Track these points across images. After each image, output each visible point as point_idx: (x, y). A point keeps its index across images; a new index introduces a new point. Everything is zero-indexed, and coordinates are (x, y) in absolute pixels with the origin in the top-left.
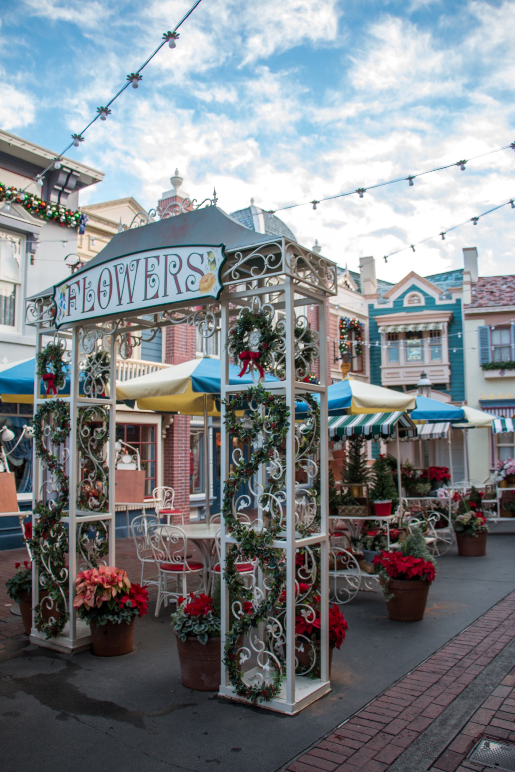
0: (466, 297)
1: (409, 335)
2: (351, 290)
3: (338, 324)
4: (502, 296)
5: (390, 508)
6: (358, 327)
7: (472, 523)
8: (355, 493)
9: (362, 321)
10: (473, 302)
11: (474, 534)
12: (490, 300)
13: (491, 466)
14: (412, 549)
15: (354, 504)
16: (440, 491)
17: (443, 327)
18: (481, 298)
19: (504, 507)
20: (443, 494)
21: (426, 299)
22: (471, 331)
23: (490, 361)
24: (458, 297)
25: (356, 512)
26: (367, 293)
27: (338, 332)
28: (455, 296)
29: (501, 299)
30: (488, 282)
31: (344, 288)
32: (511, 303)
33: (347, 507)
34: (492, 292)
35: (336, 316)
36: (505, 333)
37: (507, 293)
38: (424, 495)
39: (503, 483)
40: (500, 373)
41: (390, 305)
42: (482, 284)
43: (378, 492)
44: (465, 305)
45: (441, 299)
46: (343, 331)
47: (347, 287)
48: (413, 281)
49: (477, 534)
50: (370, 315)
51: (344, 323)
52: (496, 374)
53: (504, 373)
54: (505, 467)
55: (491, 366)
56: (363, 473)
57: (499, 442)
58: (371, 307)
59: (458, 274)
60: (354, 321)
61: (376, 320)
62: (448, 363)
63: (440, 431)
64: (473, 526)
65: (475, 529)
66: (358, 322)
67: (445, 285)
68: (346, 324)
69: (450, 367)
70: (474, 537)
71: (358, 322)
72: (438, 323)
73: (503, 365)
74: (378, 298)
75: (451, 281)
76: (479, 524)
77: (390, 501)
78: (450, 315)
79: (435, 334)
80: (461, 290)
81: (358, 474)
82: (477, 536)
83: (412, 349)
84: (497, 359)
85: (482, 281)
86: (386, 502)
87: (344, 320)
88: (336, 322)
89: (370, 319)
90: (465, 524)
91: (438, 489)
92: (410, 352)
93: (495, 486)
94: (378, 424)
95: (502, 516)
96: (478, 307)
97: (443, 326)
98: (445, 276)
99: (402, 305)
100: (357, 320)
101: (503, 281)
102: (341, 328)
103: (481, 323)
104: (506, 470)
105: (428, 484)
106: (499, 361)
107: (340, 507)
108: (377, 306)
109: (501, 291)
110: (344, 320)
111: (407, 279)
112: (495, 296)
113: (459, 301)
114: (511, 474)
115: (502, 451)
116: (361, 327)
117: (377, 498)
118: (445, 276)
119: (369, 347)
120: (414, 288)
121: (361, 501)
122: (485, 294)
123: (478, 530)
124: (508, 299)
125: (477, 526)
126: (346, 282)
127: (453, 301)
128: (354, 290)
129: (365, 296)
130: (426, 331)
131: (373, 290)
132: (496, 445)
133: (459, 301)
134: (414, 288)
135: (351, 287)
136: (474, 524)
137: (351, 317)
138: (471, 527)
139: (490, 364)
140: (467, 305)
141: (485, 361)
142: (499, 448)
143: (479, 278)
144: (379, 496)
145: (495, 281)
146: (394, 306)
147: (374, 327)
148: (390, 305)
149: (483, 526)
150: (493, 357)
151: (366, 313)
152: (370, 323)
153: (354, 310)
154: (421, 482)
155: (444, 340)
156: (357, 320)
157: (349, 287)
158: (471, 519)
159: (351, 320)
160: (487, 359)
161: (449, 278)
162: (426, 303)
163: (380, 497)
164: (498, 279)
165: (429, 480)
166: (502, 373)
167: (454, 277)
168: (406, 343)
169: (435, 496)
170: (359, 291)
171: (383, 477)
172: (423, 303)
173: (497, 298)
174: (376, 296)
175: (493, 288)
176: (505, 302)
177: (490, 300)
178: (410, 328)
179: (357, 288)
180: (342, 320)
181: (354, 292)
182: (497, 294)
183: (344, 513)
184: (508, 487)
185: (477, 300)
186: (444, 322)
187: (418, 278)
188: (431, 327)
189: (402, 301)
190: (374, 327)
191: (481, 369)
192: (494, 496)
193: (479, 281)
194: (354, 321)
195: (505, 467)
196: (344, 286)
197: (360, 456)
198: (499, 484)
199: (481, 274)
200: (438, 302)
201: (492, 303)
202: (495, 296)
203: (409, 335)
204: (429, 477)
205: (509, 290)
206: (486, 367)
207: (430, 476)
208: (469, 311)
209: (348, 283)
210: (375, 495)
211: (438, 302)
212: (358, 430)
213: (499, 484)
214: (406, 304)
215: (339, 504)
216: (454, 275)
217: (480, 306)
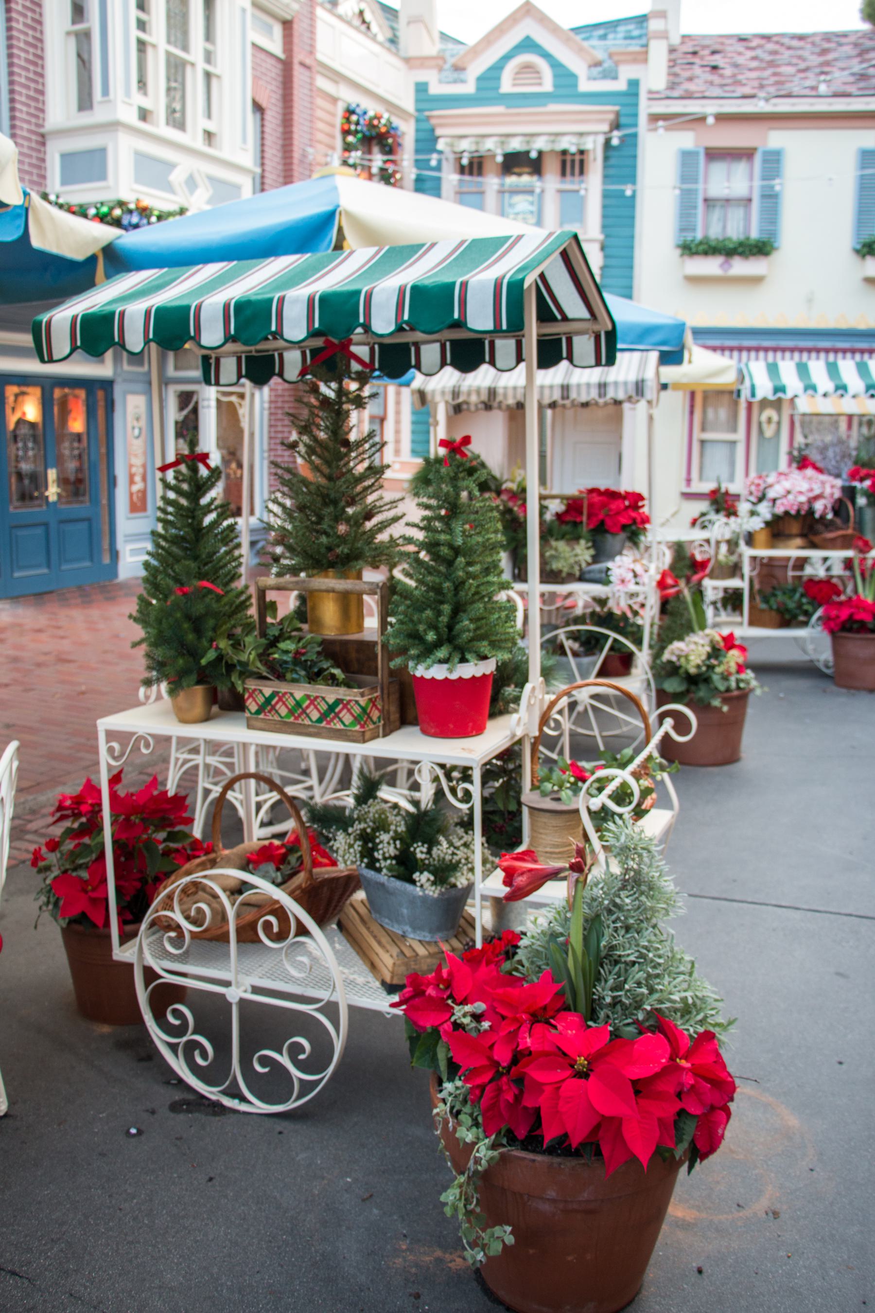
0: (654, 75)
1: (514, 162)
2: (374, 38)
3: (339, 121)
4: (740, 77)
5: (490, 692)
6: (386, 135)
7: (711, 668)
8: (329, 613)
9: (396, 122)
10: (672, 86)
11: (716, 703)
12: (711, 83)
13: (684, 483)
14: (610, 957)
15: (315, 676)
16: (622, 565)
17: (594, 145)
18: (690, 79)
19: (758, 599)
20: (630, 575)
21: (556, 76)
22: (660, 156)
23: (699, 235)
24: (633, 76)
25: (323, 717)
26: (413, 52)
27: (339, 143)
28: (627, 72)
29: (738, 83)
30: (704, 47)
31: (357, 29)
32: (762, 94)
33: (283, 688)
34: (715, 68)
35: (334, 100)
36: (740, 168)
37: (750, 70)
38: (570, 578)
39: (762, 538)
40: (721, 266)
41: (469, 88)
42: (691, 50)
43: (433, 626)
44: (650, 92)
45: (591, 78)
46: (350, 139)
47: (363, 28)
48: (528, 28)
49: (725, 701)
50: (418, 110)
51: (354, 118)
52: (711, 266)
53: (730, 266)
54: (771, 494)
55: (701, 248)
56: (369, 525)
57: (703, 429)
58: (421, 88)
59: (631, 27)
60: (378, 117)
61: (433, 121)
62: (601, 237)
63: (632, 377)
64: (716, 678)
65: (722, 687)
66: (389, 121)
67: (598, 49)
68: (357, 123)
69: (603, 248)
70: (718, 710)
71: (389, 121)
72: (581, 134)
73: (731, 246)
74: (441, 69)
75: (616, 42)
76: (733, 668)
77: (488, 667)
78: (611, 117)
79: (572, 164)
80: (642, 57)
81: (342, 528)
82: (725, 709)
83: (517, 199)
84: (715, 233)
85: (691, 43)
86: (469, 670)
87: (353, 112)
88: (333, 115)
89: (418, 120)
90: (693, 671)
91: (611, 557)
92: (511, 206)
93: (737, 544)
94: (446, 279)
95: (752, 623)
96: (682, 98)
97: (595, 142)
98: (601, 32)
99: (498, 88)
100: (386, 116)
101: (740, 47)
102: (346, 132)
103: (687, 140)
104: (774, 501)
105: (582, 542)
106: (721, 238)
107: (251, 684)
108: (435, 89)
109: (736, 66)
110: (353, 112)
111: (513, 19)
112: (722, 76)
113: (634, 84)
114: (787, 513)
115: (709, 449)
116: (394, 137)
117: (427, 652)
118: (601, 32)
119: (413, 177)
120: (528, 45)
121: (348, 660)
122: (697, 71)
123: (728, 690)
124: (756, 84)
125: (725, 677)
126: (361, 13)
127: (620, 85)
128: (380, 38)
129: (407, 60)
130: (552, 152)
131: (431, 48)
132: (697, 435)
133: (634, 84)
134: (528, 45)
135: (374, 28)
136: (718, 670)
137: (372, 108)
138: (707, 680)
139: (701, 243)
140: (657, 92)
141: (689, 237)
142: (703, 442)
143: (684, 37)
144: (437, 645)
145: (722, 44)
146: (478, 89)
147: (427, 141)
148: (469, 88)
149: (742, 676)
150: (706, 226)
151: (408, 103)
152: (417, 131)
153: (380, 91)
154: (562, 537)
155: (594, 183)
156: (386, 116)
157: (368, 28)
158: (709, 656)
159: (371, 113)
160: (694, 230)
161: (611, 36)
162: (556, 86)
163: (442, 653)
164: (727, 42)
165: (584, 529)
166: (726, 265)
167: (621, 35)
168: (502, 185)
169: (606, 582)
170: (394, 41)
171: (457, 551)
172: (548, 85)
173: (729, 81)
174: (437, 62)
175: (717, 60)
176: (747, 90)
177: (711, 83)
178: (516, 145)
179: (389, 35)
180: (349, 112)
181: (380, 44)
182: (728, 72)
183: (266, 715)
184: (772, 546)
185: (679, 84)
186: (596, 133)
187: (543, 20)
188: (568, 144)
189: (498, 79)
190: (427, 141)
191: (678, 252)
192: (735, 570)
193: (683, 43)
194: (378, 117)
195: (771, 494)
196: (357, 22)
197: (346, 443)
198: (750, 539)
199: (687, 29)
200: (585, 86)
201: (717, 92)
202: (722, 76)
203: (514, 162)
204: (584, 518)
205: (755, 64)
206: (689, 249)
207: (589, 516)
208: (660, 108)
209: (368, 16)
210: (416, 637)
211: (585, 86)
212: (338, 315)
213: (750, 539)
214: (507, 86)
215: (246, 673)
216: (622, 29)
217: (688, 96)
